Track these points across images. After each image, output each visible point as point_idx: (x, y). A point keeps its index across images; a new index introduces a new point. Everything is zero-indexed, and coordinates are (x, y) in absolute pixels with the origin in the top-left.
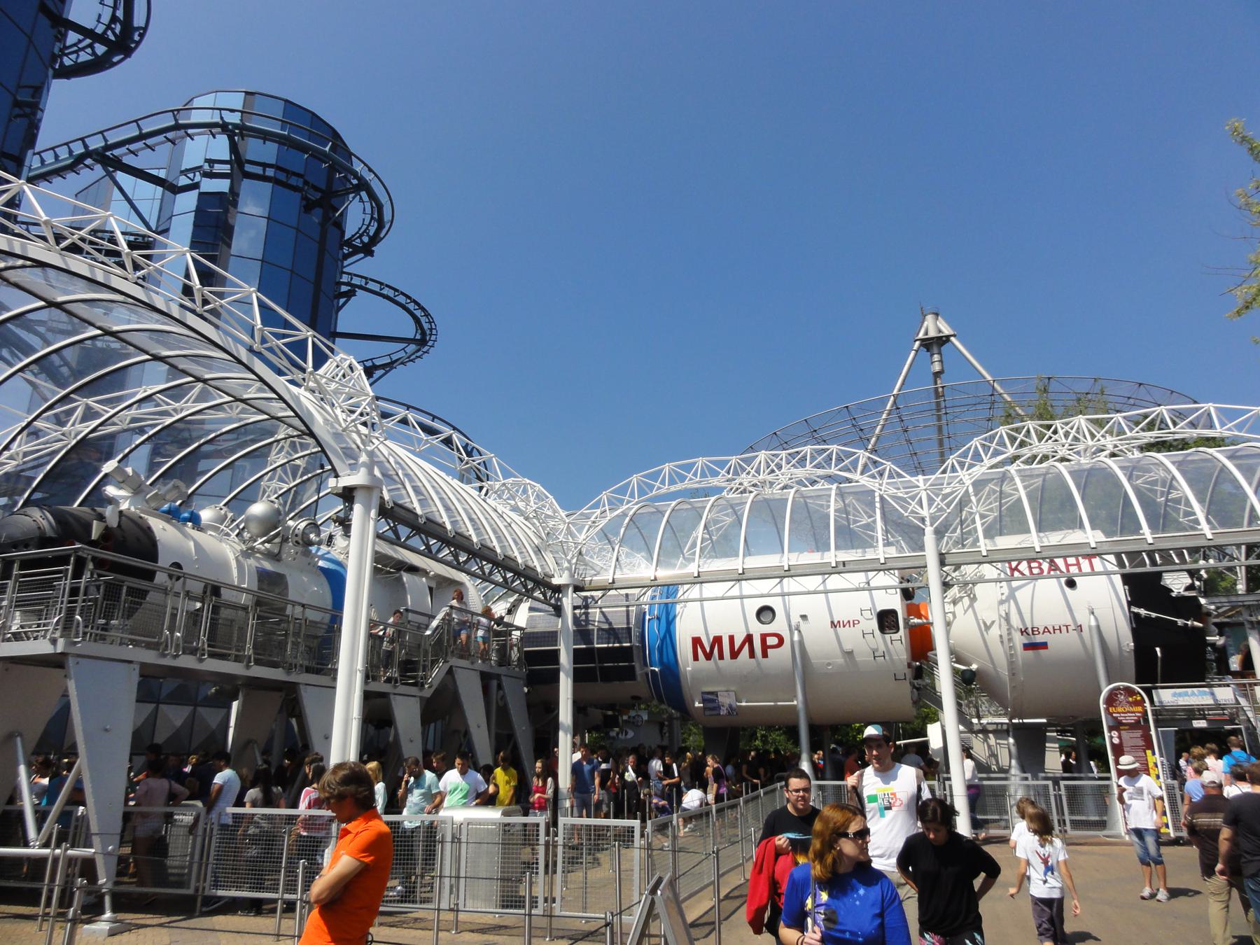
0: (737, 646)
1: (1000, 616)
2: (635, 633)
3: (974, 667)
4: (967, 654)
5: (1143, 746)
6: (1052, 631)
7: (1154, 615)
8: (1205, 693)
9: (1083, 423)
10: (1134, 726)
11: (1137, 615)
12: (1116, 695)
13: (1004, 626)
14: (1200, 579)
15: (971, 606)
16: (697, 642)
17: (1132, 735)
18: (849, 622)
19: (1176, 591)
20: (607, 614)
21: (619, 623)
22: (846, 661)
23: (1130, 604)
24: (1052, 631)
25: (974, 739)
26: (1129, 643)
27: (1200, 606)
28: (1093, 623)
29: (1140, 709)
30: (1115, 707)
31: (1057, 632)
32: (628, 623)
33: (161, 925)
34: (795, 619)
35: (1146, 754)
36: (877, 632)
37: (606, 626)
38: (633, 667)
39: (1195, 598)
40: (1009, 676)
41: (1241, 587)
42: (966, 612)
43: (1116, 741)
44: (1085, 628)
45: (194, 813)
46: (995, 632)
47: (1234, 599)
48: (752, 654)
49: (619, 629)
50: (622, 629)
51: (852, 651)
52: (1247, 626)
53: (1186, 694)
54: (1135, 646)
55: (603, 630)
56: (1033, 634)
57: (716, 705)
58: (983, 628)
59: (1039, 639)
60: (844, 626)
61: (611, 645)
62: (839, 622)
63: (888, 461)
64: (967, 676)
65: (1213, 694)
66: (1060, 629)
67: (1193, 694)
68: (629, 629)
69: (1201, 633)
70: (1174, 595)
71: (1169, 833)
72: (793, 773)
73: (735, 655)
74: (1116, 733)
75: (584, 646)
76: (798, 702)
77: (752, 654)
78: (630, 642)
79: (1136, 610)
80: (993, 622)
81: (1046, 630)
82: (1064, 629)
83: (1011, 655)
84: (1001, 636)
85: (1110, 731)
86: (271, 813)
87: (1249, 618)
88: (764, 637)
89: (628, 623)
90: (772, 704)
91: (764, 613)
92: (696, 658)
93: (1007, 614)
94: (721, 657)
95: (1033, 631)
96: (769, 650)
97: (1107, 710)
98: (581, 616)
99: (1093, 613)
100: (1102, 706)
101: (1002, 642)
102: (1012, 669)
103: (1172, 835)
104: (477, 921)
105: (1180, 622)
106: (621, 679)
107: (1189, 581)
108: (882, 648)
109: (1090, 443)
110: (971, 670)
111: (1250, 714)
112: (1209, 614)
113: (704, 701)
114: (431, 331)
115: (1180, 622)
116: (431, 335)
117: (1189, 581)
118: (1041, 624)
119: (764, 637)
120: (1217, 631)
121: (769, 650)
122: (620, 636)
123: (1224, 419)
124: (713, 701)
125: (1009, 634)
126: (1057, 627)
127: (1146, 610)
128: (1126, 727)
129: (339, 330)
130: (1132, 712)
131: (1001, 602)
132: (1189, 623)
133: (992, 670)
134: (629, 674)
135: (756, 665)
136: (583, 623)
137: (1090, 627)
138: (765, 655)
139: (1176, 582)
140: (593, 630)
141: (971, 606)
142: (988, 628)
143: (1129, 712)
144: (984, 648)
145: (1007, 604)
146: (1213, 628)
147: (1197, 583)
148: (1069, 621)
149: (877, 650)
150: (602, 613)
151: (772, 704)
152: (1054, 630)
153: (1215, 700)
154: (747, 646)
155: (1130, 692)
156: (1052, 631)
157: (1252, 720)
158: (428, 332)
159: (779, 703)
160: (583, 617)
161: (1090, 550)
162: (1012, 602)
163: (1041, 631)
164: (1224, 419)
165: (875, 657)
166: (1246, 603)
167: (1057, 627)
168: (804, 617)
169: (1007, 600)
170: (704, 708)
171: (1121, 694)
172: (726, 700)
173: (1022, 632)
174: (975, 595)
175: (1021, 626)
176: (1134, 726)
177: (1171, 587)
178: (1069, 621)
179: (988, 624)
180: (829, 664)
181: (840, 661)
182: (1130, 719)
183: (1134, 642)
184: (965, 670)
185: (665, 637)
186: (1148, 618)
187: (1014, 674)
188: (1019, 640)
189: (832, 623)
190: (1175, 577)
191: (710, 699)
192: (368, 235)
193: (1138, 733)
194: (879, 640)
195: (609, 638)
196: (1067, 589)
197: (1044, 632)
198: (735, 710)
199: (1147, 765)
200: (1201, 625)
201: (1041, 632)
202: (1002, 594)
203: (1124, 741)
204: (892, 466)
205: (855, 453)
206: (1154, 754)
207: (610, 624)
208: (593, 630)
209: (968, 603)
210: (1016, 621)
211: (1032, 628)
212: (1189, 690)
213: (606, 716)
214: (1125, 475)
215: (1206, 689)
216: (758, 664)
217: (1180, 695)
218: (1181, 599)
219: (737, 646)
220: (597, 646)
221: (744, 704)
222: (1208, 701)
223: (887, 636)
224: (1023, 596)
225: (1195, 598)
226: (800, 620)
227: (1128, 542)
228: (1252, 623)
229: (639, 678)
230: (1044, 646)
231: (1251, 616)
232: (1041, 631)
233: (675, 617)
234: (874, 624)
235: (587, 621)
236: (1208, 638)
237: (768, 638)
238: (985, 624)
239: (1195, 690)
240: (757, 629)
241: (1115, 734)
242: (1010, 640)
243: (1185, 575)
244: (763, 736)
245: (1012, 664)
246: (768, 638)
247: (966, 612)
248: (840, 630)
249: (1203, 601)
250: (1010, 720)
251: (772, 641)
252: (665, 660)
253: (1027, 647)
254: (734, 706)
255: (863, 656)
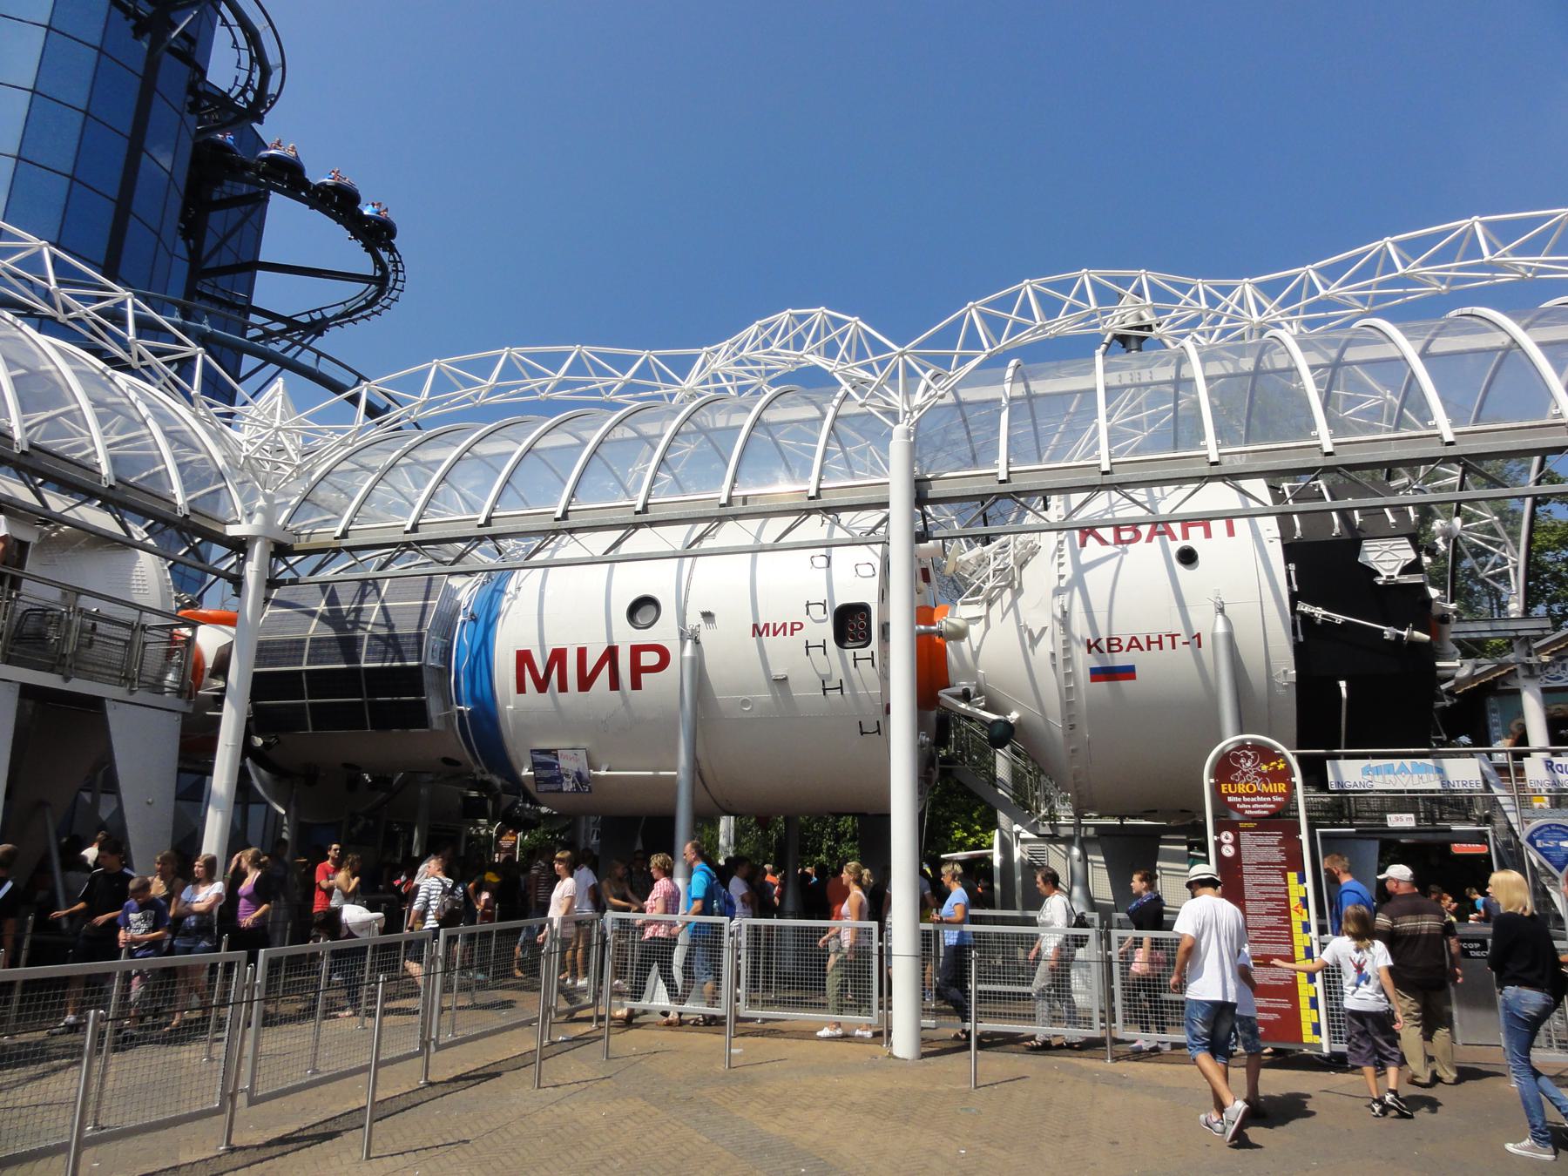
0: (590, 667)
1: (1054, 616)
2: (432, 642)
3: (1013, 716)
4: (1003, 694)
5: (1283, 863)
6: (1145, 646)
7: (1339, 619)
8: (1426, 769)
9: (1249, 290)
10: (1262, 824)
11: (1308, 619)
12: (1237, 759)
13: (1060, 638)
14: (1432, 551)
15: (1013, 604)
16: (524, 658)
17: (1260, 840)
18: (784, 625)
19: (1385, 574)
20: (391, 612)
21: (405, 627)
22: (775, 698)
23: (1294, 598)
24: (1144, 644)
25: (1050, 852)
26: (1286, 668)
27: (1429, 601)
28: (1221, 628)
29: (1282, 787)
30: (1233, 783)
31: (1155, 647)
32: (420, 626)
33: (31, 1079)
34: (694, 619)
35: (1286, 880)
36: (832, 645)
37: (383, 632)
38: (423, 704)
39: (1420, 588)
40: (1063, 728)
41: (1515, 607)
42: (1004, 615)
43: (1228, 851)
44: (1206, 640)
45: (957, 932)
46: (1045, 647)
47: (1502, 625)
48: (615, 683)
49: (403, 636)
50: (409, 636)
51: (786, 679)
52: (1521, 672)
53: (1390, 770)
54: (1298, 675)
55: (377, 637)
56: (1110, 651)
57: (555, 773)
58: (1028, 643)
59: (1120, 659)
60: (775, 634)
61: (387, 664)
62: (767, 626)
63: (853, 316)
64: (998, 730)
65: (1440, 771)
66: (1160, 642)
67: (1403, 770)
68: (420, 636)
69: (1425, 656)
70: (1380, 581)
71: (1321, 1045)
72: (541, 892)
73: (585, 683)
74: (1230, 835)
75: (345, 666)
76: (680, 771)
77: (615, 683)
78: (419, 659)
79: (1305, 608)
80: (1044, 629)
81: (1134, 643)
82: (1167, 641)
83: (1069, 690)
84: (1053, 655)
85: (1217, 832)
86: (988, 931)
87: (1525, 659)
88: (636, 651)
89: (420, 626)
90: (651, 773)
91: (642, 610)
92: (521, 688)
93: (1064, 613)
94: (563, 687)
95: (1109, 645)
96: (643, 676)
97: (1216, 789)
98: (348, 615)
99: (1222, 610)
100: (1207, 781)
101: (1054, 666)
102: (1071, 717)
103: (1326, 1050)
104: (794, 1041)
105: (1389, 632)
106: (406, 725)
107: (1412, 556)
108: (838, 674)
109: (1256, 318)
110: (1007, 723)
111: (1513, 818)
112: (1444, 619)
113: (536, 766)
114: (396, 266)
115: (1389, 632)
116: (397, 271)
117: (1412, 556)
118: (1123, 632)
119: (636, 651)
120: (1459, 653)
121: (643, 676)
122: (404, 648)
123: (1496, 242)
124: (550, 766)
125: (1066, 650)
126: (1154, 638)
127: (1325, 609)
128: (1251, 825)
129: (261, 259)
130: (1265, 795)
131: (1058, 592)
132: (1405, 633)
133: (1041, 721)
134: (418, 716)
135: (621, 702)
136: (349, 626)
137: (1214, 636)
138: (636, 684)
139: (1387, 556)
140: (362, 638)
141: (1013, 604)
142: (1034, 641)
143: (1258, 794)
144: (1029, 682)
145: (1067, 596)
146: (1452, 648)
147: (1427, 560)
148: (1178, 627)
149: (829, 677)
150: (384, 609)
151: (651, 773)
152: (1149, 643)
153: (1444, 782)
154: (606, 668)
155: (1266, 754)
156: (1145, 646)
157: (1516, 827)
158: (390, 268)
159: (661, 773)
160: (352, 617)
161: (1207, 467)
162: (1076, 590)
163: (1125, 644)
164: (1496, 242)
165: (824, 690)
166: (1520, 633)
167: (1154, 638)
168: (708, 616)
169: (1069, 588)
170: (537, 779)
171: (1247, 757)
172: (569, 764)
173: (1089, 648)
174: (1020, 584)
175: (1088, 636)
176: (1262, 824)
177: (1376, 566)
178: (1178, 627)
179: (1036, 635)
180: (745, 702)
181: (766, 696)
182: (1262, 807)
183: (1296, 669)
184: (995, 722)
185: (479, 652)
186: (1328, 625)
187: (1072, 727)
188: (1084, 661)
189: (755, 626)
190: (1386, 548)
191: (546, 761)
192: (253, 89)
193: (1274, 838)
194: (834, 660)
195: (386, 652)
196: (1179, 568)
197: (1130, 646)
198: (587, 783)
199: (1287, 902)
200: (1427, 637)
201: (1125, 648)
202: (1061, 577)
203: (1244, 853)
204: (860, 323)
205: (808, 316)
206: (1302, 880)
207: (391, 627)
208: (362, 638)
209: (1010, 599)
210: (1080, 627)
211: (1109, 640)
212: (1397, 762)
213: (467, 799)
214: (1318, 384)
215: (1429, 762)
216: (626, 702)
217: (1377, 771)
218: (1393, 588)
219: (590, 667)
220: (364, 665)
221: (603, 773)
222: (1431, 783)
223: (849, 653)
224: (1096, 581)
225: (1420, 588)
226: (701, 621)
227: (1285, 451)
228: (1529, 667)
229: (436, 724)
230: (1128, 672)
231: (1529, 655)
232: (1125, 644)
233: (498, 615)
234: (827, 631)
235: (356, 624)
236: (1439, 664)
237: (644, 655)
238: (1031, 633)
239: (1407, 762)
240: (626, 636)
241: (1227, 837)
242: (1067, 662)
243: (1405, 543)
244: (829, 847)
245: (1068, 705)
246: (644, 655)
247: (1004, 615)
248: (768, 640)
249: (1434, 593)
250: (1122, 822)
251: (650, 658)
252: (478, 692)
253: (1100, 674)
254: (585, 775)
255: (805, 689)
